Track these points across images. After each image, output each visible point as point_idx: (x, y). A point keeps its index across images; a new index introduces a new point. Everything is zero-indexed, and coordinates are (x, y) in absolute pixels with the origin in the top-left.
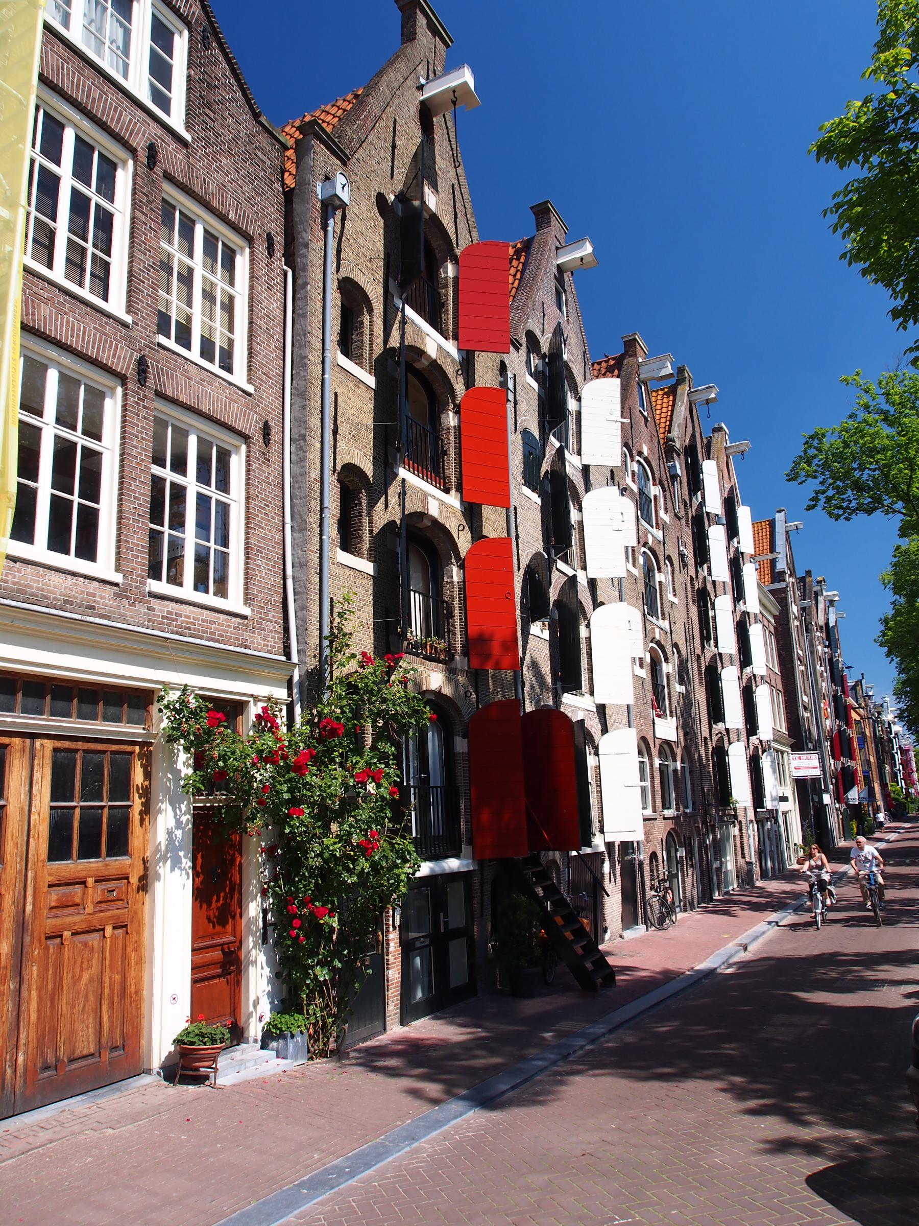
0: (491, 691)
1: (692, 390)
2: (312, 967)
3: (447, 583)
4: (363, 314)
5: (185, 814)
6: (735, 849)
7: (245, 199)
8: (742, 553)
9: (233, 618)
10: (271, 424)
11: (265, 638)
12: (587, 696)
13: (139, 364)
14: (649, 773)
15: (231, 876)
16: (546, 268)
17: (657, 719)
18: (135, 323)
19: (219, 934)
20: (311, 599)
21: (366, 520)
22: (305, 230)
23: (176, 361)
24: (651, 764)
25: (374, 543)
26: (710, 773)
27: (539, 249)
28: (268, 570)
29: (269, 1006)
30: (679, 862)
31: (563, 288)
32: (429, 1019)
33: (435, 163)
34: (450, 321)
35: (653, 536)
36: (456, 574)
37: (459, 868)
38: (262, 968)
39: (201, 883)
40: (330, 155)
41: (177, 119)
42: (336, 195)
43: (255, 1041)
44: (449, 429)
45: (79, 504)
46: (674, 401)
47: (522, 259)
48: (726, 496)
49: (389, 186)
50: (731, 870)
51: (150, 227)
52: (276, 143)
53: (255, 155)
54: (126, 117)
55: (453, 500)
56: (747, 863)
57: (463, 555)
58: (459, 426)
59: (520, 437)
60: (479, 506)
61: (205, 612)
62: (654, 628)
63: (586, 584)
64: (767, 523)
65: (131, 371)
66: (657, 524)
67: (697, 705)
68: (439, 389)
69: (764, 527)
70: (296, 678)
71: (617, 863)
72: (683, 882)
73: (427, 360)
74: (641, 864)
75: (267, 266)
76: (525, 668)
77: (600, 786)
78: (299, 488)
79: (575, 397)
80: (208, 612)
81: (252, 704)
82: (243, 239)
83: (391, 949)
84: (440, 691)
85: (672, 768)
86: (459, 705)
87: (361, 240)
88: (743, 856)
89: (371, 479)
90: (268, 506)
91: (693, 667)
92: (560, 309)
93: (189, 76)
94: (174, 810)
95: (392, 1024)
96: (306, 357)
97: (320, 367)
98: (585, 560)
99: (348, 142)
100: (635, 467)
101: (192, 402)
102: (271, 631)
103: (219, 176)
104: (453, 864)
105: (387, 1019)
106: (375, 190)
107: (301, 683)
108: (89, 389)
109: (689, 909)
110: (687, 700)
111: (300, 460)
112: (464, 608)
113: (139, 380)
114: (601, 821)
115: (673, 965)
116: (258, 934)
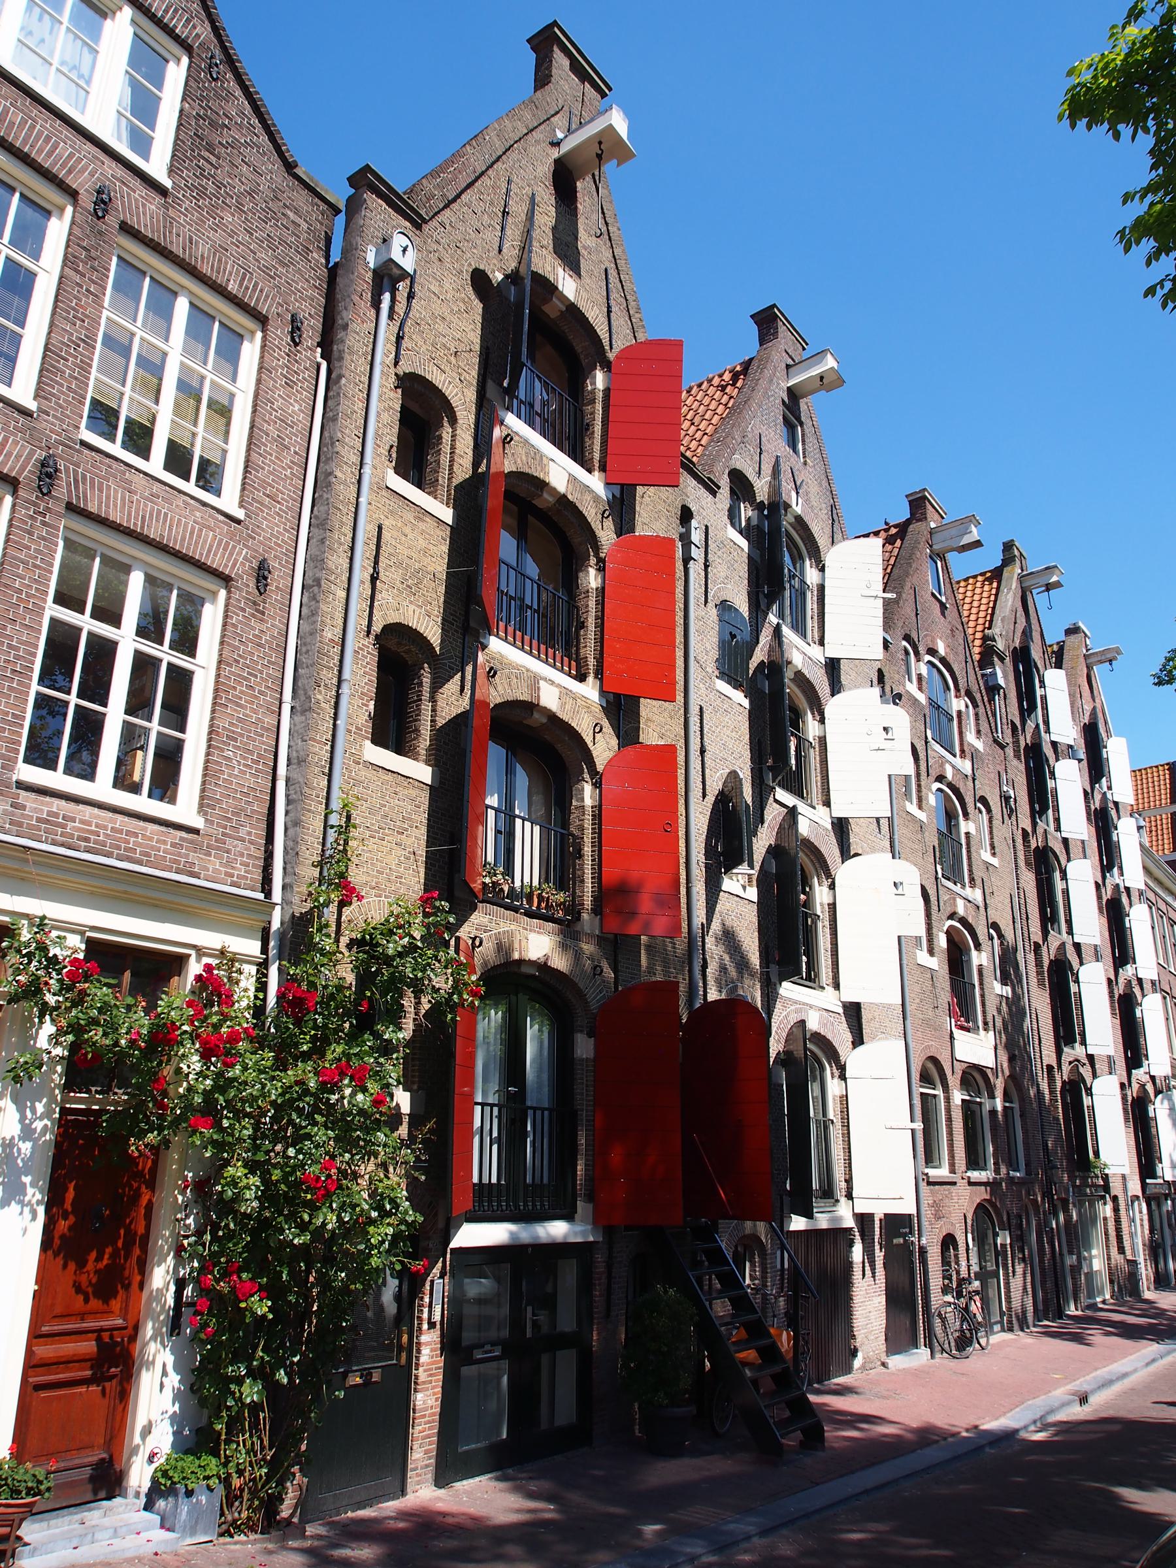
0: (643, 969)
1: (1025, 573)
2: (240, 1381)
3: (576, 808)
4: (443, 426)
5: (41, 1118)
6: (1107, 1239)
7: (258, 267)
8: (1116, 804)
9: (172, 831)
10: (273, 564)
11: (229, 864)
12: (830, 990)
13: (43, 465)
14: (943, 1113)
15: (131, 1223)
16: (767, 390)
17: (957, 1033)
18: (40, 409)
19: (95, 1313)
20: (309, 811)
21: (426, 707)
22: (346, 309)
23: (110, 467)
24: (948, 1099)
25: (436, 740)
26: (1058, 1119)
27: (758, 367)
28: (246, 766)
29: (171, 1438)
30: (1000, 1253)
31: (798, 419)
32: (490, 1479)
33: (577, 238)
34: (597, 447)
35: (953, 767)
36: (588, 794)
37: (566, 1236)
38: (165, 1373)
39: (70, 1228)
40: (393, 213)
41: (157, 166)
42: (391, 260)
43: (137, 1495)
44: (588, 592)
45: (159, 733)
46: (998, 588)
47: (739, 384)
48: (1087, 721)
49: (496, 262)
50: (1100, 1271)
51: (88, 290)
52: (319, 202)
53: (283, 214)
54: (63, 150)
55: (590, 690)
56: (1128, 1261)
57: (600, 768)
58: (603, 588)
59: (714, 612)
60: (634, 702)
61: (120, 818)
62: (954, 899)
63: (829, 827)
64: (1166, 767)
65: (27, 474)
66: (962, 751)
67: (1034, 1016)
68: (576, 539)
69: (1161, 773)
70: (276, 925)
71: (877, 1247)
72: (1007, 1284)
73: (551, 495)
74: (923, 1251)
75: (288, 355)
76: (710, 941)
77: (848, 1126)
78: (307, 652)
79: (817, 566)
80: (126, 819)
81: (193, 959)
82: (251, 318)
83: (424, 1359)
84: (545, 963)
85: (987, 1107)
86: (581, 985)
87: (441, 327)
88: (1121, 1250)
89: (437, 649)
90: (256, 676)
91: (1026, 961)
92: (795, 450)
93: (181, 111)
94: (21, 1110)
95: (418, 1483)
96: (331, 473)
97: (354, 489)
98: (829, 792)
99: (424, 199)
100: (924, 669)
101: (133, 524)
102: (242, 855)
103: (218, 237)
104: (557, 1230)
105: (409, 1474)
106: (470, 264)
107: (282, 935)
108: (105, 560)
109: (1016, 1326)
110: (1015, 1010)
111: (309, 614)
112: (598, 844)
113: (39, 487)
114: (849, 1181)
115: (941, 1420)
116: (162, 1318)
